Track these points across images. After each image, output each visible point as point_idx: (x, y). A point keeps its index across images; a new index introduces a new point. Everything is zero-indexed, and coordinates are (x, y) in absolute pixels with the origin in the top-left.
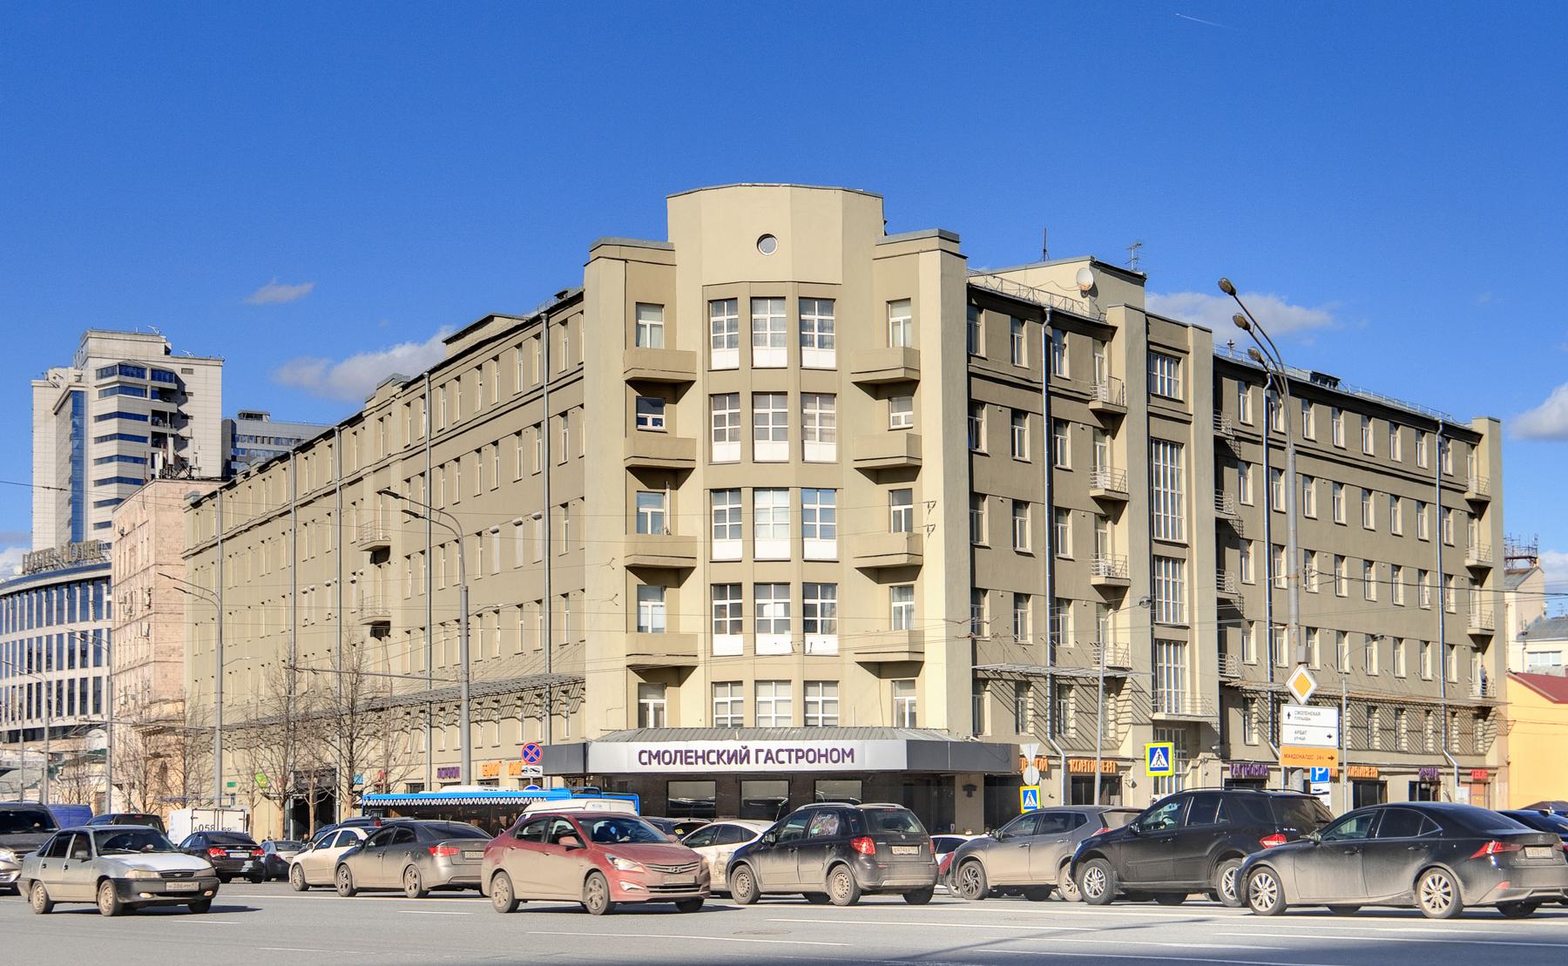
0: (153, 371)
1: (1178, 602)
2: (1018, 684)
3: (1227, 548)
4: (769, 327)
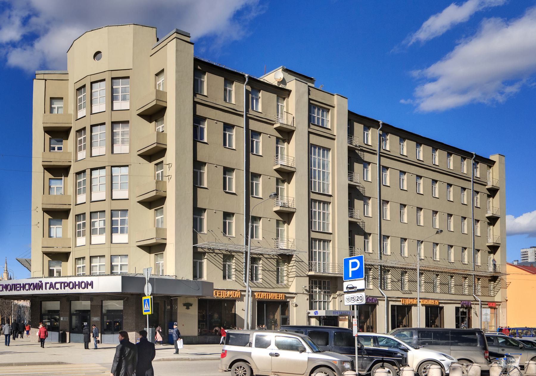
1: (326, 222)
2: (225, 255)
3: (355, 199)
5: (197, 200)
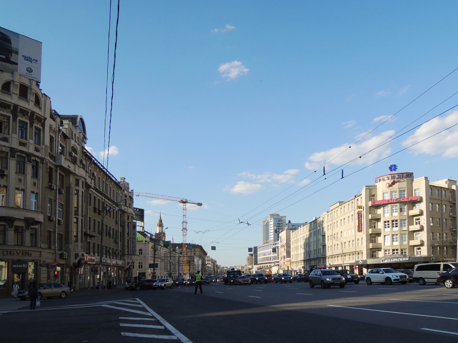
0: (142, 265)
4: (401, 193)
5: (127, 326)
